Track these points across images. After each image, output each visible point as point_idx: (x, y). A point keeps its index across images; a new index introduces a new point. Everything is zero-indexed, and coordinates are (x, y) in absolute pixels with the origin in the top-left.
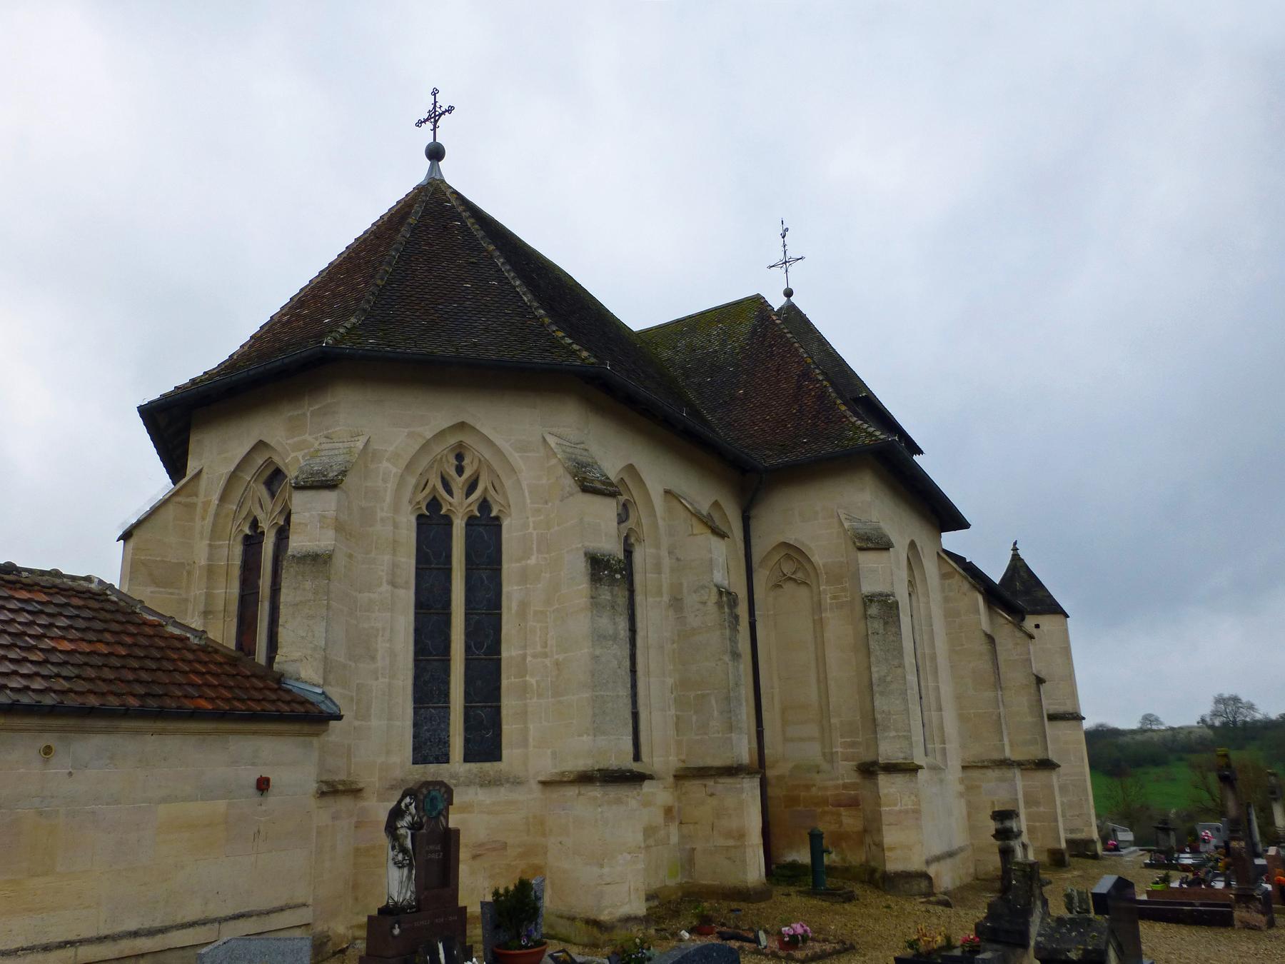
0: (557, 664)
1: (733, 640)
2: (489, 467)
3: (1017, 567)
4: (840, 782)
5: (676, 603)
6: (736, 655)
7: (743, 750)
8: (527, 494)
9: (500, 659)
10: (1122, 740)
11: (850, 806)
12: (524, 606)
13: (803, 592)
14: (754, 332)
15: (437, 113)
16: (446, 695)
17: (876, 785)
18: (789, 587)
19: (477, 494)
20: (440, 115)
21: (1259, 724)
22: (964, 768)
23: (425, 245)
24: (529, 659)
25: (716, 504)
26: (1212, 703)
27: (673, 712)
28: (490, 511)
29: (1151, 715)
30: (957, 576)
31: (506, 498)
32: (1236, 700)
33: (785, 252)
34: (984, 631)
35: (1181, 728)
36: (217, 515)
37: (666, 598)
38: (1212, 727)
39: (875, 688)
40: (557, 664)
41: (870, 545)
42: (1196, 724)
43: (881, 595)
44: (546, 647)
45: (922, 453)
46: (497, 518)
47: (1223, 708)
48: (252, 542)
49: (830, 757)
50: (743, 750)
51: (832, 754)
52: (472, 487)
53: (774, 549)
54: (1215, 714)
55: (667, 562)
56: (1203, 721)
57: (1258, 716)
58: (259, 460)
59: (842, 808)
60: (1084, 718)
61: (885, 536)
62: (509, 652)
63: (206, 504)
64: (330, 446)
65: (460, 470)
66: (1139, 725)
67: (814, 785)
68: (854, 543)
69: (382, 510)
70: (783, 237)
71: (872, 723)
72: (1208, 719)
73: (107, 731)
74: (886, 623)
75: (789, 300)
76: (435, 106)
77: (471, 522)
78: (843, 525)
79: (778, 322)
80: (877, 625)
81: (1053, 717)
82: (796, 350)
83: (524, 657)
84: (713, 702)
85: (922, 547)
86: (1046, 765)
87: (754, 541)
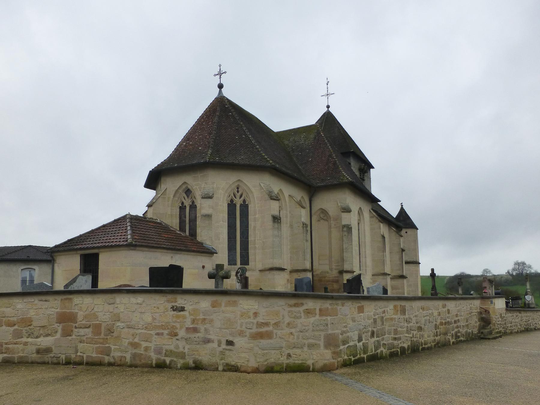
0: (263, 242)
1: (306, 237)
2: (246, 191)
3: (402, 212)
4: (334, 276)
5: (291, 226)
6: (307, 241)
7: (308, 266)
8: (255, 199)
9: (248, 240)
10: (472, 279)
11: (336, 282)
12: (255, 227)
13: (326, 223)
14: (315, 138)
15: (221, 73)
16: (235, 249)
17: (343, 276)
18: (322, 221)
19: (242, 198)
20: (222, 74)
21: (533, 275)
22: (373, 275)
23: (223, 123)
24: (256, 240)
25: (302, 197)
26: (513, 264)
27: (289, 255)
28: (246, 202)
29: (487, 269)
30: (375, 218)
31: (250, 200)
32: (524, 263)
33: (328, 91)
34: (381, 234)
35: (498, 275)
36: (172, 201)
37: (288, 225)
38: (512, 275)
39: (344, 250)
40: (263, 242)
41: (345, 211)
42: (505, 274)
43: (347, 225)
44: (260, 238)
45: (374, 168)
46: (247, 204)
47: (518, 267)
48: (182, 208)
49: (331, 269)
50: (308, 266)
51: (332, 268)
52: (241, 196)
53: (318, 210)
54: (514, 270)
55: (289, 215)
56: (508, 272)
57: (533, 271)
58: (184, 187)
59: (334, 283)
60: (420, 264)
61: (350, 208)
62: (251, 239)
63: (169, 198)
64: (207, 186)
65: (238, 192)
66: (482, 274)
67: (326, 277)
68: (341, 210)
69: (220, 202)
70: (327, 85)
71: (342, 260)
72: (510, 272)
73: (188, 255)
74: (348, 233)
75: (328, 110)
76: (220, 70)
77: (241, 205)
78: (338, 205)
79: (323, 135)
80: (346, 233)
81: (407, 263)
82: (328, 146)
83: (255, 240)
84: (300, 253)
85: (363, 209)
86: (402, 277)
87: (313, 207)
